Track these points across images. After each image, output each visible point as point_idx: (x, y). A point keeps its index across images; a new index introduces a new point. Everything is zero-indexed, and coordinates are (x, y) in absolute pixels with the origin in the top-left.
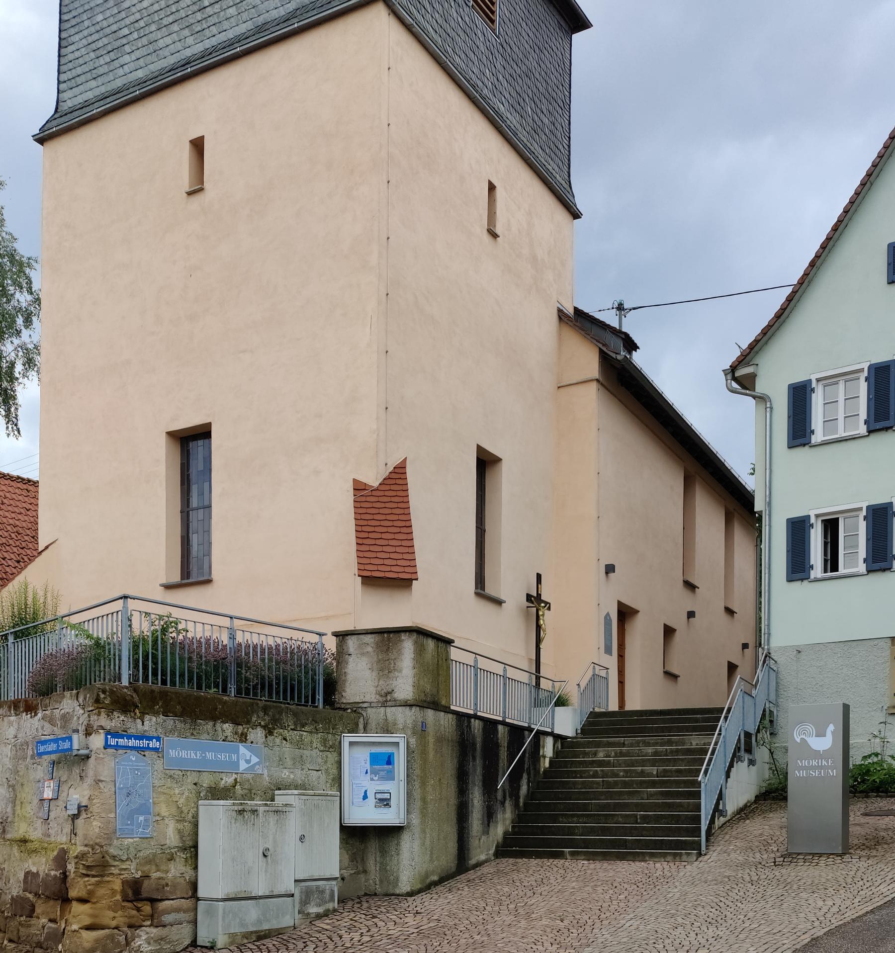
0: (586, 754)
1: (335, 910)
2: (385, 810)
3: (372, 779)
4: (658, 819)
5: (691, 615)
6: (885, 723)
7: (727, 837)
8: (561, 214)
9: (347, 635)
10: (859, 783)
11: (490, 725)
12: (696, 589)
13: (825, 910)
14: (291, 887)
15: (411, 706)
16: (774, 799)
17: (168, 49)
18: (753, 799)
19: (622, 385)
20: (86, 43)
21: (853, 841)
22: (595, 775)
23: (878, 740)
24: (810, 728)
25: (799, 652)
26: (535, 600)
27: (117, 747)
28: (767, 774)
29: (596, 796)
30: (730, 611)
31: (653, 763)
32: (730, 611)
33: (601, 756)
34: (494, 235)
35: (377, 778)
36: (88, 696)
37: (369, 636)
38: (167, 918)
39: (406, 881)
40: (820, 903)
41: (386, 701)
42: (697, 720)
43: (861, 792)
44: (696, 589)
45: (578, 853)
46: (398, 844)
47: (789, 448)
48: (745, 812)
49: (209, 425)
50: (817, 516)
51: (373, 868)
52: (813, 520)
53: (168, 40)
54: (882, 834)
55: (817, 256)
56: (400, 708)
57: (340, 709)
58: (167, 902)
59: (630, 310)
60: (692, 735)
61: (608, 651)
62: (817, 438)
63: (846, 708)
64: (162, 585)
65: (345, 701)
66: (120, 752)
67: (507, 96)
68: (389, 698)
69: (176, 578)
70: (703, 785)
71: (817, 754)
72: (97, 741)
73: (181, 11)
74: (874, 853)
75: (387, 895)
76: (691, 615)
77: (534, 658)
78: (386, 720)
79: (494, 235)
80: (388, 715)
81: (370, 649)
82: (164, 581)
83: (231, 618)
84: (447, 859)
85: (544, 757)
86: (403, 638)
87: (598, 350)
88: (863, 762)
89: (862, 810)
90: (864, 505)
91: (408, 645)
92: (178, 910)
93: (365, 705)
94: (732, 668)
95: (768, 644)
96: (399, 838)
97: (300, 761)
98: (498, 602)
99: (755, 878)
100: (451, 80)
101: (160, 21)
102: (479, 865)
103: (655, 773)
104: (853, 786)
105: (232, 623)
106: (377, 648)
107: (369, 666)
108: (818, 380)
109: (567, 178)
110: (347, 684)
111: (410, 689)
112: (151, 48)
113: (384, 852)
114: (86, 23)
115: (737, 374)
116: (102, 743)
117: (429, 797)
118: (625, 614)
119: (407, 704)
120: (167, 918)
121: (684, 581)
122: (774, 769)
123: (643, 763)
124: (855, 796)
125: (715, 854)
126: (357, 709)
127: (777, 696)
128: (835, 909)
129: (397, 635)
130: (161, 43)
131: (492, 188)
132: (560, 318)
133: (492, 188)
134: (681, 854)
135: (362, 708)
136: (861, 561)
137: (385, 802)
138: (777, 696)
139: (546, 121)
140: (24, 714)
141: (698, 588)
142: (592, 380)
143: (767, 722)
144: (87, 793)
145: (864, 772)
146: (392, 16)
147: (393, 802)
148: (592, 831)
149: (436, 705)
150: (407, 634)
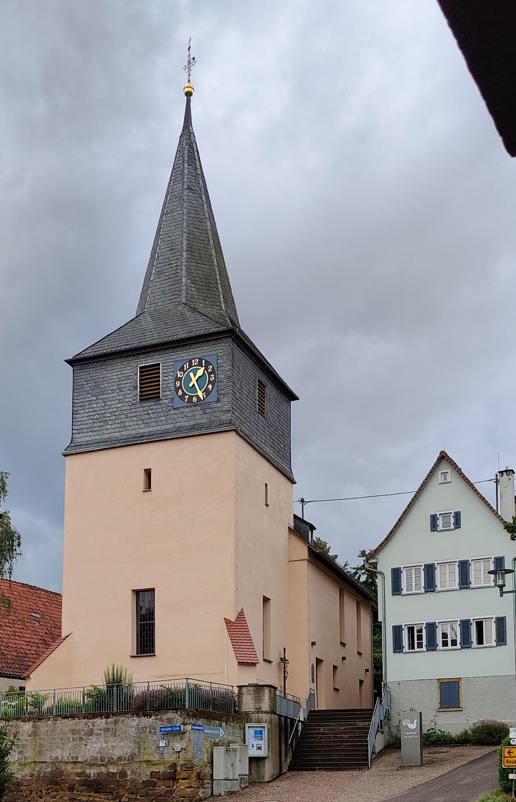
0: (315, 730)
1: (248, 787)
2: (260, 751)
4: (350, 755)
5: (344, 658)
6: (436, 716)
7: (377, 762)
8: (289, 483)
10: (426, 741)
11: (286, 718)
13: (416, 781)
14: (237, 777)
15: (268, 713)
16: (391, 748)
17: (131, 427)
18: (383, 748)
20: (87, 415)
21: (424, 762)
22: (321, 738)
23: (433, 723)
24: (409, 721)
25: (399, 684)
26: (284, 660)
27: (194, 729)
28: (387, 737)
29: (323, 747)
30: (360, 654)
31: (345, 733)
32: (360, 654)
36: (183, 713)
38: (206, 786)
39: (267, 778)
40: (415, 779)
41: (259, 711)
43: (427, 745)
45: (322, 769)
46: (264, 763)
47: (393, 595)
48: (381, 753)
51: (254, 772)
52: (403, 627)
53: (131, 423)
54: (435, 759)
56: (264, 714)
57: (240, 714)
58: (205, 781)
59: (308, 502)
60: (356, 721)
61: (313, 682)
63: (421, 713)
67: (269, 442)
68: (259, 710)
69: (135, 654)
70: (369, 742)
71: (411, 730)
72: (189, 727)
74: (432, 765)
75: (260, 782)
76: (344, 658)
77: (283, 685)
79: (267, 505)
80: (259, 716)
81: (252, 692)
82: (131, 655)
83: (211, 683)
84: (277, 770)
85: (299, 731)
86: (265, 688)
89: (428, 752)
91: (267, 691)
92: (208, 783)
93: (250, 713)
94: (361, 682)
95: (386, 680)
96: (264, 761)
97: (234, 733)
98: (270, 662)
99: (392, 774)
102: (284, 773)
103: (346, 737)
104: (424, 743)
105: (211, 685)
106: (255, 691)
107: (252, 698)
110: (243, 705)
111: (268, 707)
113: (258, 767)
114: (88, 407)
115: (369, 562)
116: (190, 728)
117: (273, 746)
118: (319, 661)
119: (266, 712)
120: (206, 786)
121: (340, 642)
123: (340, 733)
125: (374, 768)
126: (247, 714)
127: (390, 703)
128: (420, 780)
130: (127, 424)
131: (266, 485)
133: (266, 485)
134: (362, 768)
137: (259, 748)
138: (390, 703)
139: (282, 446)
140: (143, 717)
142: (305, 560)
143: (387, 715)
144: (185, 744)
145: (428, 736)
147: (262, 748)
148: (325, 760)
149: (275, 713)
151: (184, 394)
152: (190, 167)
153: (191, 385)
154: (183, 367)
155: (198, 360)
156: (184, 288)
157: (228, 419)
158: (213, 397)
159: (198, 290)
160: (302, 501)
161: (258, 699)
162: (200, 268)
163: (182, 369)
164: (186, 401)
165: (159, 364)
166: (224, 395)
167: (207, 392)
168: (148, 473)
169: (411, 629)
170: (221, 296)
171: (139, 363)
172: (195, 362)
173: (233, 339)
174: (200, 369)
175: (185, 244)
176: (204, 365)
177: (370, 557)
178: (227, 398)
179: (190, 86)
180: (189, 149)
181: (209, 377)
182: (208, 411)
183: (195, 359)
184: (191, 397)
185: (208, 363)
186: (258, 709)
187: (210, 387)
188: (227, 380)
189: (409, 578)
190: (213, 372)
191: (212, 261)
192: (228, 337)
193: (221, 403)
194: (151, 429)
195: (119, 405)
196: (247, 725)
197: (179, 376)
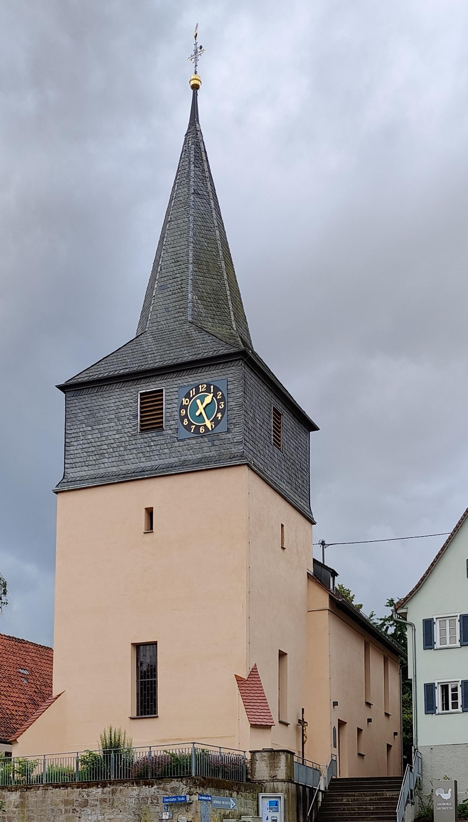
3: (270, 812)
5: (369, 720)
8: (307, 524)
9: (256, 752)
10: (462, 813)
11: (305, 787)
12: (371, 706)
15: (285, 782)
17: (130, 461)
19: (338, 609)
22: (344, 810)
24: (442, 790)
25: (432, 749)
26: (302, 722)
27: (201, 800)
28: (418, 809)
30: (387, 715)
32: (387, 715)
33: (345, 801)
34: (283, 548)
35: (271, 811)
36: (189, 781)
37: (266, 753)
41: (274, 780)
42: (385, 783)
43: (463, 817)
44: (371, 706)
47: (424, 649)
49: (157, 642)
50: (438, 683)
52: (436, 685)
53: (131, 457)
55: (434, 561)
56: (280, 783)
59: (329, 545)
60: (383, 791)
61: (335, 747)
62: (437, 646)
64: (129, 718)
65: (255, 779)
66: (202, 801)
67: (286, 478)
68: (275, 778)
69: (135, 715)
70: (397, 814)
71: (445, 801)
73: (138, 445)
78: (274, 787)
80: (275, 785)
82: (130, 716)
83: (220, 748)
87: (328, 595)
88: (463, 803)
90: (460, 680)
91: (283, 757)
93: (265, 781)
94: (389, 747)
95: (417, 745)
97: (246, 804)
98: (287, 724)
100: (268, 485)
101: (126, 447)
103: (372, 809)
104: (459, 815)
105: (220, 750)
106: (269, 757)
108: (437, 618)
109: (309, 505)
110: (256, 772)
111: (285, 775)
112: (121, 458)
116: (197, 799)
118: (341, 724)
119: (282, 781)
122: (422, 806)
123: (366, 804)
124: (460, 819)
127: (422, 770)
129: (278, 753)
131: (282, 526)
132: (308, 577)
133: (282, 526)
135: (263, 782)
136: (458, 641)
138: (422, 770)
139: (300, 482)
140: (144, 786)
141: (372, 705)
143: (418, 784)
146: (250, 470)
150: (283, 752)
151: (190, 424)
152: (197, 169)
153: (197, 414)
154: (189, 393)
155: (205, 386)
156: (190, 305)
157: (240, 451)
158: (223, 427)
159: (205, 307)
160: (323, 544)
161: (273, 766)
162: (208, 283)
163: (187, 396)
164: (192, 431)
165: (162, 390)
166: (235, 424)
167: (216, 421)
168: (150, 512)
169: (445, 688)
170: (232, 313)
171: (140, 389)
172: (202, 388)
173: (245, 362)
174: (208, 395)
175: (191, 255)
176: (212, 391)
177: (399, 607)
178: (238, 429)
179: (197, 78)
180: (196, 149)
181: (219, 405)
182: (217, 443)
183: (202, 384)
184: (198, 428)
185: (217, 389)
186: (274, 777)
187: (219, 415)
188: (238, 408)
189: (443, 631)
190: (223, 399)
191: (222, 274)
192: (240, 359)
193: (231, 434)
194: (153, 463)
195: (117, 436)
196: (261, 795)
197: (184, 403)
